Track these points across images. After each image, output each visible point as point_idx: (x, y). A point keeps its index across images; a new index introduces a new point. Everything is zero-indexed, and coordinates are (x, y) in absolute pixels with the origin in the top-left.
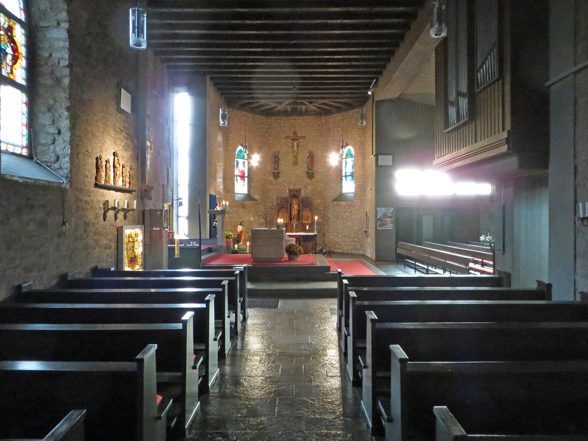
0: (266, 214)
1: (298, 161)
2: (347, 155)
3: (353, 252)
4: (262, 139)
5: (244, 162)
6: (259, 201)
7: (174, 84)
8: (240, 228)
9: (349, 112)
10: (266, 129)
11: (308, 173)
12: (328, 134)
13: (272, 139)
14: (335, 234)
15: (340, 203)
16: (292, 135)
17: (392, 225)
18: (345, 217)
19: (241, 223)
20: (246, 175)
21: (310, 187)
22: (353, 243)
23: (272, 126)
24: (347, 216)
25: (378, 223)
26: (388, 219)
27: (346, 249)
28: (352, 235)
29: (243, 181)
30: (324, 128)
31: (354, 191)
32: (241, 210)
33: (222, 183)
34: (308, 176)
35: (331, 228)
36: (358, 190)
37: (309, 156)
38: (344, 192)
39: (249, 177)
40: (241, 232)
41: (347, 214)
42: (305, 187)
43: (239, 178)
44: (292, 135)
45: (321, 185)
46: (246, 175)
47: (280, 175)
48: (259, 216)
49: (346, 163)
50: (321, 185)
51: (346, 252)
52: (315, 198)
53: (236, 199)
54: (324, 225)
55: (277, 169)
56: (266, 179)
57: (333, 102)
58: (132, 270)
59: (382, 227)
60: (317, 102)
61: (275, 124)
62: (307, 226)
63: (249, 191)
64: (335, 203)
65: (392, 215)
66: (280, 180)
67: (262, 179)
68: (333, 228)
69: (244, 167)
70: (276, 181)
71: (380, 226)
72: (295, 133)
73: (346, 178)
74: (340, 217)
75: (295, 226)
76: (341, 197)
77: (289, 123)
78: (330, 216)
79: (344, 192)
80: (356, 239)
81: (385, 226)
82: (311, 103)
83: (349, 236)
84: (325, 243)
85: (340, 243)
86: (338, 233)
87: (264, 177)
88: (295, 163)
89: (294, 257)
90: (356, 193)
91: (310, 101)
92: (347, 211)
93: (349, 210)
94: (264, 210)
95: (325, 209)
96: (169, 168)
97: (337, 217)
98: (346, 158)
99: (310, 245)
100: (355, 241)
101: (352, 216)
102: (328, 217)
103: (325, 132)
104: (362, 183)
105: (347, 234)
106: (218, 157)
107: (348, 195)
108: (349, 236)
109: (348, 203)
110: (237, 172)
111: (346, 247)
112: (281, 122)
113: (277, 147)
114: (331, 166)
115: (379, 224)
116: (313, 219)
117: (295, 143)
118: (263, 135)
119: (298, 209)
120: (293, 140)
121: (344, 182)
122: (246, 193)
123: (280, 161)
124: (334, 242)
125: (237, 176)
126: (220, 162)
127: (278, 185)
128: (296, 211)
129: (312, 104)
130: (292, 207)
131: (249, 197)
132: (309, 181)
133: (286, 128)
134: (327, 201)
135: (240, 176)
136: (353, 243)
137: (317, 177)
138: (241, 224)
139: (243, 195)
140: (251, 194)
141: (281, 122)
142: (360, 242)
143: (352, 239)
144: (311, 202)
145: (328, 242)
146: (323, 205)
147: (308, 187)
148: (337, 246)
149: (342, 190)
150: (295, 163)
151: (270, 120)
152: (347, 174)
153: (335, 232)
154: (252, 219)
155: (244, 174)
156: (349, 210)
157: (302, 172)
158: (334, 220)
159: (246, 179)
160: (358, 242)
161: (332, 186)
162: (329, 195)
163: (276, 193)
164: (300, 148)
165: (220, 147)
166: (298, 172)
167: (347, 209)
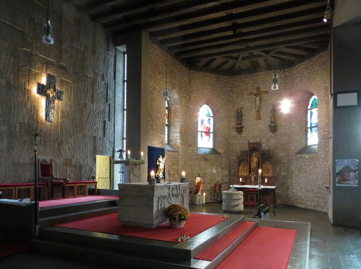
0: (230, 167)
1: (261, 115)
2: (312, 105)
3: (317, 209)
4: (227, 97)
5: (209, 119)
7: (289, 115)
8: (198, 179)
9: (312, 58)
10: (231, 88)
11: (270, 126)
12: (291, 86)
13: (236, 96)
14: (299, 188)
15: (303, 155)
16: (255, 91)
17: (357, 181)
18: (308, 170)
19: (199, 175)
21: (273, 141)
22: (317, 199)
23: (236, 84)
24: (310, 170)
25: (337, 179)
26: (352, 174)
27: (310, 205)
28: (316, 191)
29: (208, 137)
30: (288, 81)
31: (317, 143)
32: (204, 162)
33: (179, 138)
34: (271, 130)
35: (294, 181)
36: (323, 141)
37: (272, 110)
38: (309, 144)
39: (214, 133)
40: (199, 183)
41: (310, 167)
42: (268, 140)
43: (203, 134)
44: (255, 91)
45: (286, 138)
46: (212, 130)
47: (244, 130)
48: (223, 168)
49: (311, 113)
50: (286, 138)
51: (309, 208)
52: (278, 151)
53: (198, 153)
54: (288, 178)
55: (240, 124)
56: (230, 134)
57: (288, 47)
59: (342, 183)
60: (273, 50)
61: (238, 83)
62: (241, 179)
63: (214, 145)
64: (298, 155)
65: (357, 168)
66: (244, 134)
67: (226, 134)
68: (296, 181)
69: (210, 123)
70: (240, 136)
71: (339, 183)
72: (258, 89)
73: (311, 130)
74: (303, 171)
75: (253, 179)
76: (305, 149)
77: (253, 79)
78: (293, 169)
79: (309, 144)
80: (320, 195)
81: (347, 182)
82: (267, 52)
83: (312, 190)
84: (289, 197)
85: (304, 198)
86: (301, 188)
87: (229, 133)
90: (320, 145)
91: (263, 49)
92: (310, 164)
93: (312, 163)
94: (228, 163)
95: (288, 162)
96: (107, 122)
97: (300, 170)
98: (311, 109)
99: (269, 198)
100: (318, 197)
101: (315, 169)
102: (291, 171)
103: (289, 85)
104: (326, 133)
105: (310, 189)
106: (176, 114)
107: (313, 147)
108: (312, 190)
109: (312, 155)
110: (200, 128)
111: (309, 203)
112: (245, 80)
113: (241, 104)
114: (282, 113)
115: (339, 179)
116: (257, 172)
117: (258, 99)
118: (227, 93)
119: (258, 161)
120: (255, 96)
121: (309, 134)
122: (212, 147)
123: (243, 116)
124: (297, 197)
125: (202, 132)
126: (178, 118)
127: (241, 139)
128: (255, 164)
129: (269, 55)
130: (251, 160)
131: (214, 151)
132: (273, 135)
133: (249, 85)
134: (291, 154)
135: (206, 133)
136: (317, 199)
137: (280, 130)
138: (199, 176)
139: (208, 149)
140: (216, 148)
141: (245, 80)
142: (324, 199)
143: (315, 195)
144: (271, 154)
145: (291, 196)
146: (287, 159)
147: (271, 140)
148: (300, 200)
149: (307, 143)
150: (259, 118)
151: (234, 79)
152: (313, 125)
153: (297, 186)
154: (214, 171)
155: (209, 130)
156: (312, 163)
158: (297, 173)
159: (212, 135)
160: (321, 198)
161: (296, 138)
162: (293, 148)
163: (240, 147)
164: (263, 103)
165: (178, 104)
166: (262, 126)
167: (310, 162)
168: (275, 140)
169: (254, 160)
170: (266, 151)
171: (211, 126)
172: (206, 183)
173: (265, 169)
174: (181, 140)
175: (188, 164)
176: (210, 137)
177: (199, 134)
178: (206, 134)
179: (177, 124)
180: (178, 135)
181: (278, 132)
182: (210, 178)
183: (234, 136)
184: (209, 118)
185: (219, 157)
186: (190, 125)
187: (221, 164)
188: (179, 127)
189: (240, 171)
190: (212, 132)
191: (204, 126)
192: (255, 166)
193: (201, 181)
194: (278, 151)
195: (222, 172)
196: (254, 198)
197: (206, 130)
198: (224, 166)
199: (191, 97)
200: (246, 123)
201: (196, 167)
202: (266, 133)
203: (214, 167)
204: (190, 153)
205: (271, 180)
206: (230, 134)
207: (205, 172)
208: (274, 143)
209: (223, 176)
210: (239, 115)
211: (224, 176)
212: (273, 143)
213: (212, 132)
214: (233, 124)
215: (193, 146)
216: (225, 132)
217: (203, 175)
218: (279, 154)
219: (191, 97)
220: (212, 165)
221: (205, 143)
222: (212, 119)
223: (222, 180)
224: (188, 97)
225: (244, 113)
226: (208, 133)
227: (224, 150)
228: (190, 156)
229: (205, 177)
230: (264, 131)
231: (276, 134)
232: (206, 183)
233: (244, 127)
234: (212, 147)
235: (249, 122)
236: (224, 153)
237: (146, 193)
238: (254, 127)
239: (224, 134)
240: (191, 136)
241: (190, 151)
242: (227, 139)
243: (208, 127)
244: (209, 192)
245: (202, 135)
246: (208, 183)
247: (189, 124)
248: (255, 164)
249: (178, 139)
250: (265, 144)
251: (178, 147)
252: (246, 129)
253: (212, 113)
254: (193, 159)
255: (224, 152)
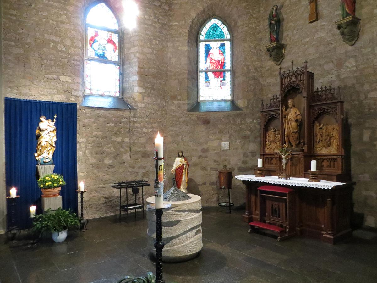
6: (245, 110)
20: (228, 66)
21: (351, 64)
32: (202, 128)
43: (211, 75)
46: (228, 66)
47: (286, 52)
48: (245, 137)
56: (261, 67)
58: (78, 197)
69: (223, 53)
87: (257, 64)
88: (315, 16)
89: (5, 229)
125: (206, 72)
132: (350, 48)
135: (215, 72)
147: (347, 64)
154: (225, 145)
155: (223, 65)
157: (330, 31)
159: (228, 75)
166: (322, 34)
168: (356, 61)
169: (290, 115)
170: (328, 88)
171: (226, 58)
172: (209, 169)
173: (321, 136)
174: (143, 87)
175: (170, 133)
176: (224, 79)
177: (202, 76)
178: (216, 75)
179: (134, 59)
180: (136, 78)
181: (365, 38)
182: (216, 159)
183: (268, 70)
184: (222, 42)
185: (237, 115)
186: (172, 59)
187: (241, 130)
188: (137, 63)
189: (267, 142)
190: (229, 69)
191: (212, 59)
192: (292, 131)
193: (183, 165)
194: (366, 87)
195: (243, 146)
196: (281, 211)
197: (216, 67)
198: (249, 133)
199: (173, 7)
200: (290, 36)
201: (187, 139)
202: (335, 47)
203: (226, 137)
204: (174, 112)
205: (336, 163)
206: (262, 67)
207: (205, 146)
208: (355, 69)
209: (245, 154)
210: (276, 24)
211: (250, 154)
212: (352, 69)
213: (229, 69)
214: (266, 42)
215: (179, 97)
216: (248, 63)
217: (201, 154)
218: (369, 96)
219: (173, 7)
220: (220, 132)
221: (215, 92)
222: (228, 45)
223: (244, 162)
224: (167, 8)
225: (285, 16)
226: (219, 72)
227: (249, 100)
228: (174, 116)
229: (206, 157)
230: (329, 43)
231: (358, 44)
232: (209, 169)
233: (286, 45)
234: (229, 98)
235: (295, 32)
236: (247, 107)
237: (63, 184)
238: (307, 40)
239: (248, 68)
240: (175, 79)
241: (173, 108)
242: (254, 79)
243: (219, 61)
244: (215, 186)
245: (207, 78)
246: (211, 168)
247: (170, 58)
248: (294, 124)
249: (136, 86)
250: (333, 76)
251: (136, 101)
252: (291, 48)
253: (227, 32)
254: (180, 122)
255: (248, 104)
